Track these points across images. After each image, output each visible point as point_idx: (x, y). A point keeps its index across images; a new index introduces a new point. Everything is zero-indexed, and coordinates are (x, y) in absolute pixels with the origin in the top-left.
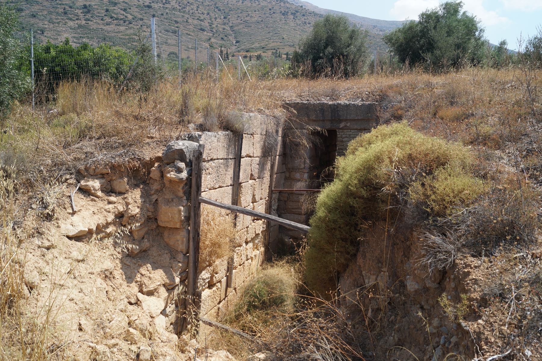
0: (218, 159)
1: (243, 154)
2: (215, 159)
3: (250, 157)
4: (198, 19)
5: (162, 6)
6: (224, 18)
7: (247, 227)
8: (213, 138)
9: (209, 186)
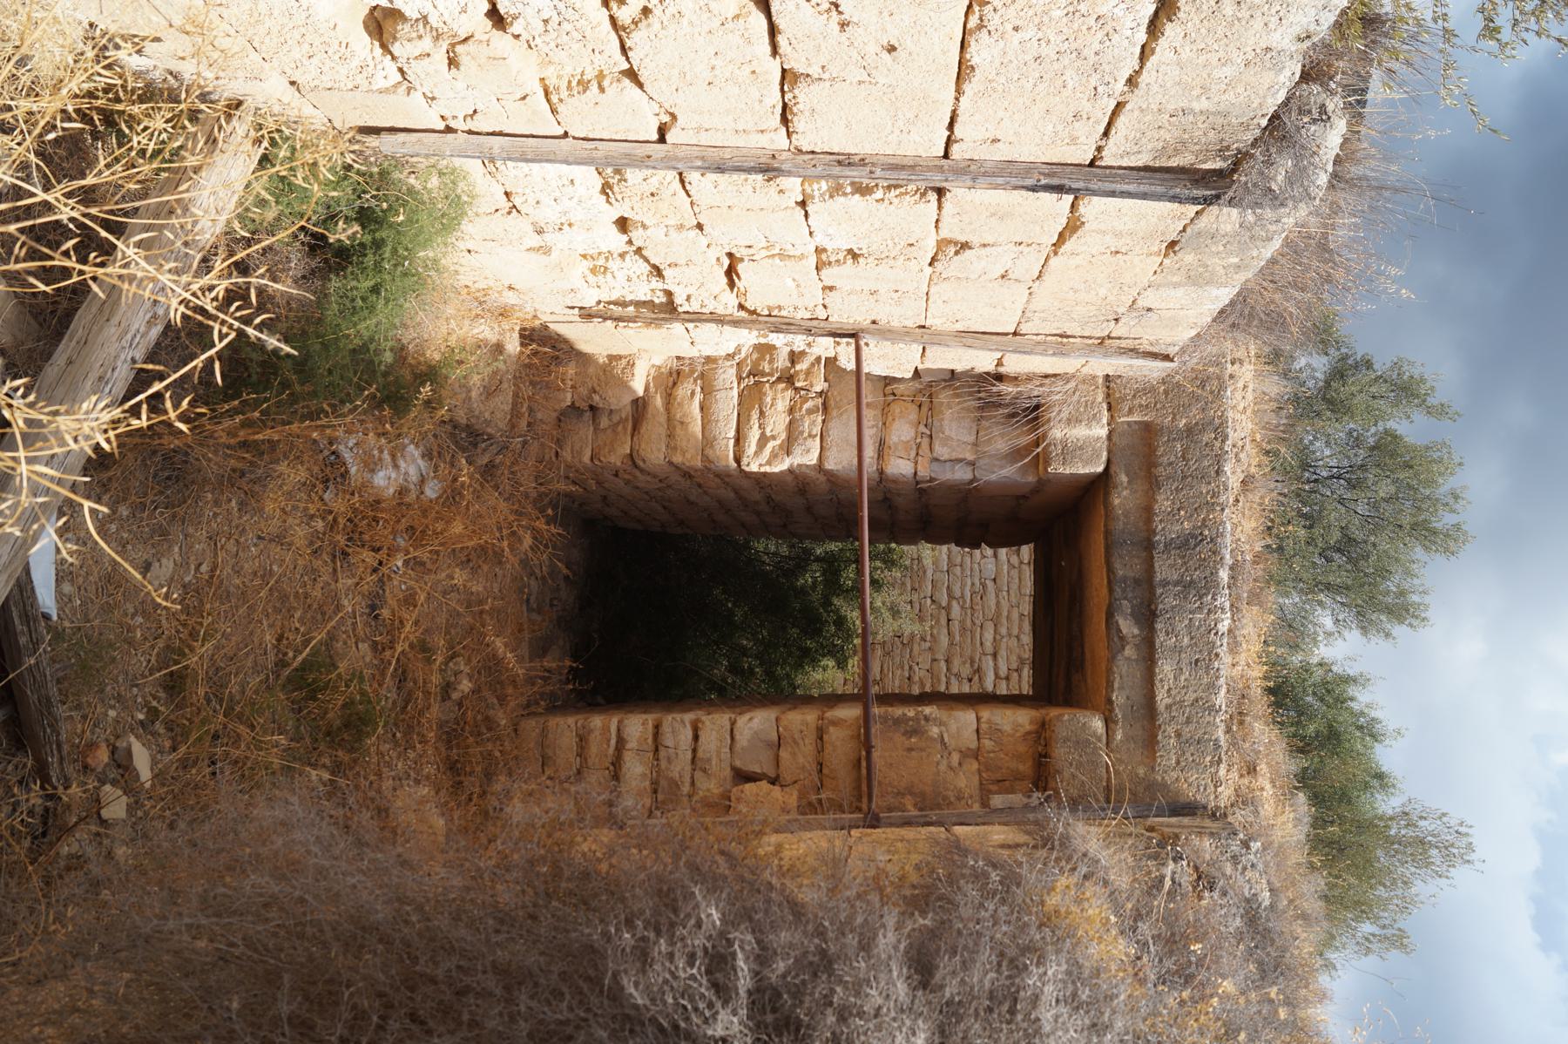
0: (1145, 53)
3: (785, 120)
7: (700, 227)
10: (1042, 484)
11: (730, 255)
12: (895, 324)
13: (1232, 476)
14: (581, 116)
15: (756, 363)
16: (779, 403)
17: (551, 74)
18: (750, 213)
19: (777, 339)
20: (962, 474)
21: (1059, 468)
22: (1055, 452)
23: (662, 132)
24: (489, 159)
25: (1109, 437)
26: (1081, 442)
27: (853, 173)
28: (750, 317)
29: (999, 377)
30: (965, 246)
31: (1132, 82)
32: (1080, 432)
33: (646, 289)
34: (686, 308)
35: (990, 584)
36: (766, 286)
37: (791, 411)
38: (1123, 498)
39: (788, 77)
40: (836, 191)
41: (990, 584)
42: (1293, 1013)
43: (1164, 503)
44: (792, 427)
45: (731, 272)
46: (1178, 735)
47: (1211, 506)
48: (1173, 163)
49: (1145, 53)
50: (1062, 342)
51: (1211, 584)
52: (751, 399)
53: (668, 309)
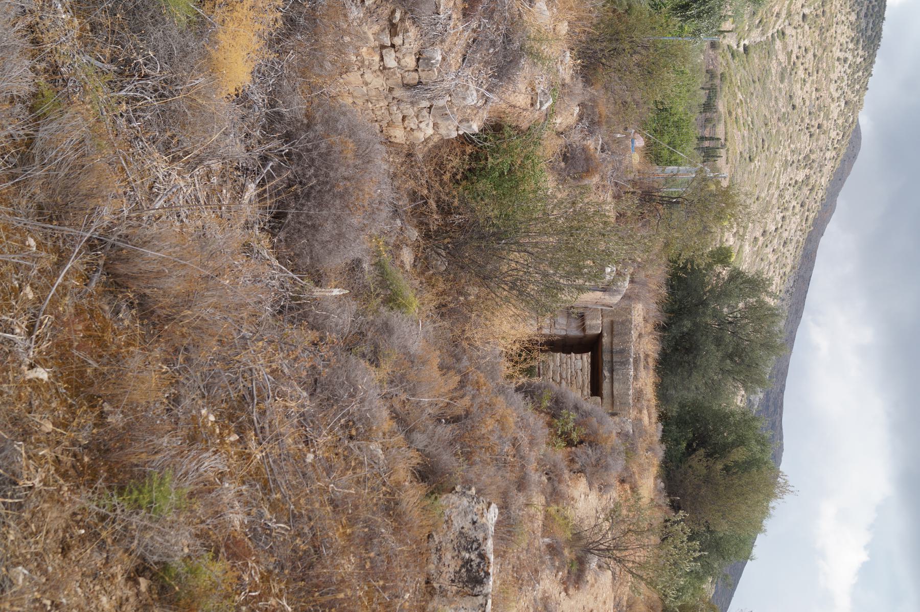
6: (804, 16)
10: (585, 336)
13: (634, 334)
22: (587, 327)
32: (594, 322)
35: (579, 371)
38: (606, 340)
41: (579, 371)
42: (466, 299)
43: (616, 341)
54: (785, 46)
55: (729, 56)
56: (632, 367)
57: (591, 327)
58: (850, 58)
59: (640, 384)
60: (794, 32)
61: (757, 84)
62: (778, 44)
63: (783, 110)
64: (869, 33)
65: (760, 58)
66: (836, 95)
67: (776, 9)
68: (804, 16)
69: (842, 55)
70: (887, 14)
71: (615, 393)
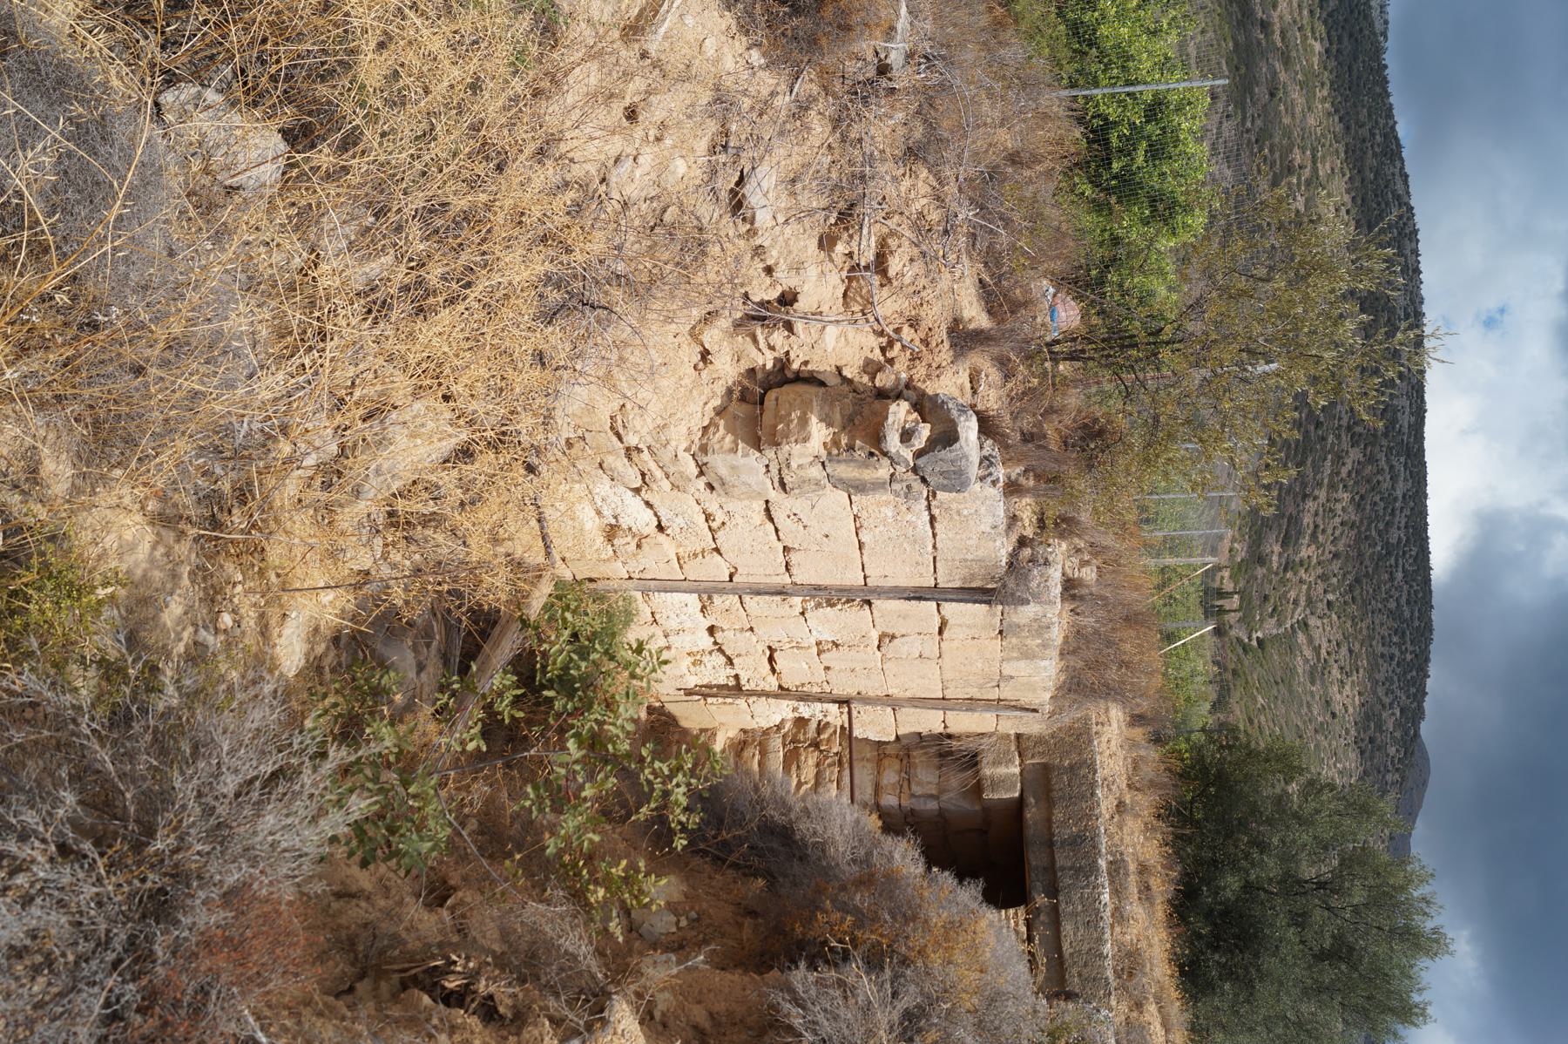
0: (934, 535)
1: (949, 609)
2: (933, 527)
3: (941, 632)
4: (1316, 526)
5: (1344, 423)
6: (1329, 603)
7: (751, 629)
8: (989, 520)
9: (864, 515)
11: (770, 648)
12: (871, 694)
13: (1105, 804)
14: (695, 571)
15: (795, 735)
16: (810, 760)
17: (681, 550)
18: (778, 621)
19: (805, 710)
20: (932, 805)
21: (988, 795)
22: (987, 783)
23: (731, 576)
24: (645, 592)
25: (1021, 773)
26: (1005, 777)
27: (828, 596)
28: (783, 692)
29: (949, 736)
30: (893, 637)
31: (934, 547)
32: (1002, 770)
33: (723, 676)
34: (747, 687)
36: (796, 669)
37: (818, 765)
38: (1031, 814)
39: (786, 549)
40: (818, 605)
43: (1058, 815)
44: (818, 776)
45: (771, 659)
46: (1080, 975)
47: (1089, 817)
48: (974, 585)
49: (934, 535)
50: (971, 704)
51: (1093, 869)
52: (791, 758)
53: (736, 689)
54: (1310, 640)
55: (1240, 651)
56: (1104, 879)
57: (996, 784)
58: (1397, 653)
59: (1131, 934)
60: (1319, 623)
61: (1281, 686)
62: (1301, 637)
63: (1320, 719)
64: (1417, 623)
65: (1280, 655)
66: (1387, 701)
67: (1292, 595)
68: (1329, 603)
69: (1385, 650)
70: (1436, 600)
71: (1067, 948)
